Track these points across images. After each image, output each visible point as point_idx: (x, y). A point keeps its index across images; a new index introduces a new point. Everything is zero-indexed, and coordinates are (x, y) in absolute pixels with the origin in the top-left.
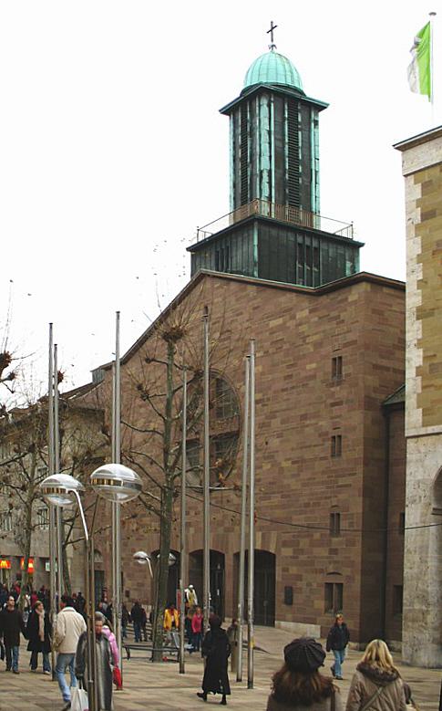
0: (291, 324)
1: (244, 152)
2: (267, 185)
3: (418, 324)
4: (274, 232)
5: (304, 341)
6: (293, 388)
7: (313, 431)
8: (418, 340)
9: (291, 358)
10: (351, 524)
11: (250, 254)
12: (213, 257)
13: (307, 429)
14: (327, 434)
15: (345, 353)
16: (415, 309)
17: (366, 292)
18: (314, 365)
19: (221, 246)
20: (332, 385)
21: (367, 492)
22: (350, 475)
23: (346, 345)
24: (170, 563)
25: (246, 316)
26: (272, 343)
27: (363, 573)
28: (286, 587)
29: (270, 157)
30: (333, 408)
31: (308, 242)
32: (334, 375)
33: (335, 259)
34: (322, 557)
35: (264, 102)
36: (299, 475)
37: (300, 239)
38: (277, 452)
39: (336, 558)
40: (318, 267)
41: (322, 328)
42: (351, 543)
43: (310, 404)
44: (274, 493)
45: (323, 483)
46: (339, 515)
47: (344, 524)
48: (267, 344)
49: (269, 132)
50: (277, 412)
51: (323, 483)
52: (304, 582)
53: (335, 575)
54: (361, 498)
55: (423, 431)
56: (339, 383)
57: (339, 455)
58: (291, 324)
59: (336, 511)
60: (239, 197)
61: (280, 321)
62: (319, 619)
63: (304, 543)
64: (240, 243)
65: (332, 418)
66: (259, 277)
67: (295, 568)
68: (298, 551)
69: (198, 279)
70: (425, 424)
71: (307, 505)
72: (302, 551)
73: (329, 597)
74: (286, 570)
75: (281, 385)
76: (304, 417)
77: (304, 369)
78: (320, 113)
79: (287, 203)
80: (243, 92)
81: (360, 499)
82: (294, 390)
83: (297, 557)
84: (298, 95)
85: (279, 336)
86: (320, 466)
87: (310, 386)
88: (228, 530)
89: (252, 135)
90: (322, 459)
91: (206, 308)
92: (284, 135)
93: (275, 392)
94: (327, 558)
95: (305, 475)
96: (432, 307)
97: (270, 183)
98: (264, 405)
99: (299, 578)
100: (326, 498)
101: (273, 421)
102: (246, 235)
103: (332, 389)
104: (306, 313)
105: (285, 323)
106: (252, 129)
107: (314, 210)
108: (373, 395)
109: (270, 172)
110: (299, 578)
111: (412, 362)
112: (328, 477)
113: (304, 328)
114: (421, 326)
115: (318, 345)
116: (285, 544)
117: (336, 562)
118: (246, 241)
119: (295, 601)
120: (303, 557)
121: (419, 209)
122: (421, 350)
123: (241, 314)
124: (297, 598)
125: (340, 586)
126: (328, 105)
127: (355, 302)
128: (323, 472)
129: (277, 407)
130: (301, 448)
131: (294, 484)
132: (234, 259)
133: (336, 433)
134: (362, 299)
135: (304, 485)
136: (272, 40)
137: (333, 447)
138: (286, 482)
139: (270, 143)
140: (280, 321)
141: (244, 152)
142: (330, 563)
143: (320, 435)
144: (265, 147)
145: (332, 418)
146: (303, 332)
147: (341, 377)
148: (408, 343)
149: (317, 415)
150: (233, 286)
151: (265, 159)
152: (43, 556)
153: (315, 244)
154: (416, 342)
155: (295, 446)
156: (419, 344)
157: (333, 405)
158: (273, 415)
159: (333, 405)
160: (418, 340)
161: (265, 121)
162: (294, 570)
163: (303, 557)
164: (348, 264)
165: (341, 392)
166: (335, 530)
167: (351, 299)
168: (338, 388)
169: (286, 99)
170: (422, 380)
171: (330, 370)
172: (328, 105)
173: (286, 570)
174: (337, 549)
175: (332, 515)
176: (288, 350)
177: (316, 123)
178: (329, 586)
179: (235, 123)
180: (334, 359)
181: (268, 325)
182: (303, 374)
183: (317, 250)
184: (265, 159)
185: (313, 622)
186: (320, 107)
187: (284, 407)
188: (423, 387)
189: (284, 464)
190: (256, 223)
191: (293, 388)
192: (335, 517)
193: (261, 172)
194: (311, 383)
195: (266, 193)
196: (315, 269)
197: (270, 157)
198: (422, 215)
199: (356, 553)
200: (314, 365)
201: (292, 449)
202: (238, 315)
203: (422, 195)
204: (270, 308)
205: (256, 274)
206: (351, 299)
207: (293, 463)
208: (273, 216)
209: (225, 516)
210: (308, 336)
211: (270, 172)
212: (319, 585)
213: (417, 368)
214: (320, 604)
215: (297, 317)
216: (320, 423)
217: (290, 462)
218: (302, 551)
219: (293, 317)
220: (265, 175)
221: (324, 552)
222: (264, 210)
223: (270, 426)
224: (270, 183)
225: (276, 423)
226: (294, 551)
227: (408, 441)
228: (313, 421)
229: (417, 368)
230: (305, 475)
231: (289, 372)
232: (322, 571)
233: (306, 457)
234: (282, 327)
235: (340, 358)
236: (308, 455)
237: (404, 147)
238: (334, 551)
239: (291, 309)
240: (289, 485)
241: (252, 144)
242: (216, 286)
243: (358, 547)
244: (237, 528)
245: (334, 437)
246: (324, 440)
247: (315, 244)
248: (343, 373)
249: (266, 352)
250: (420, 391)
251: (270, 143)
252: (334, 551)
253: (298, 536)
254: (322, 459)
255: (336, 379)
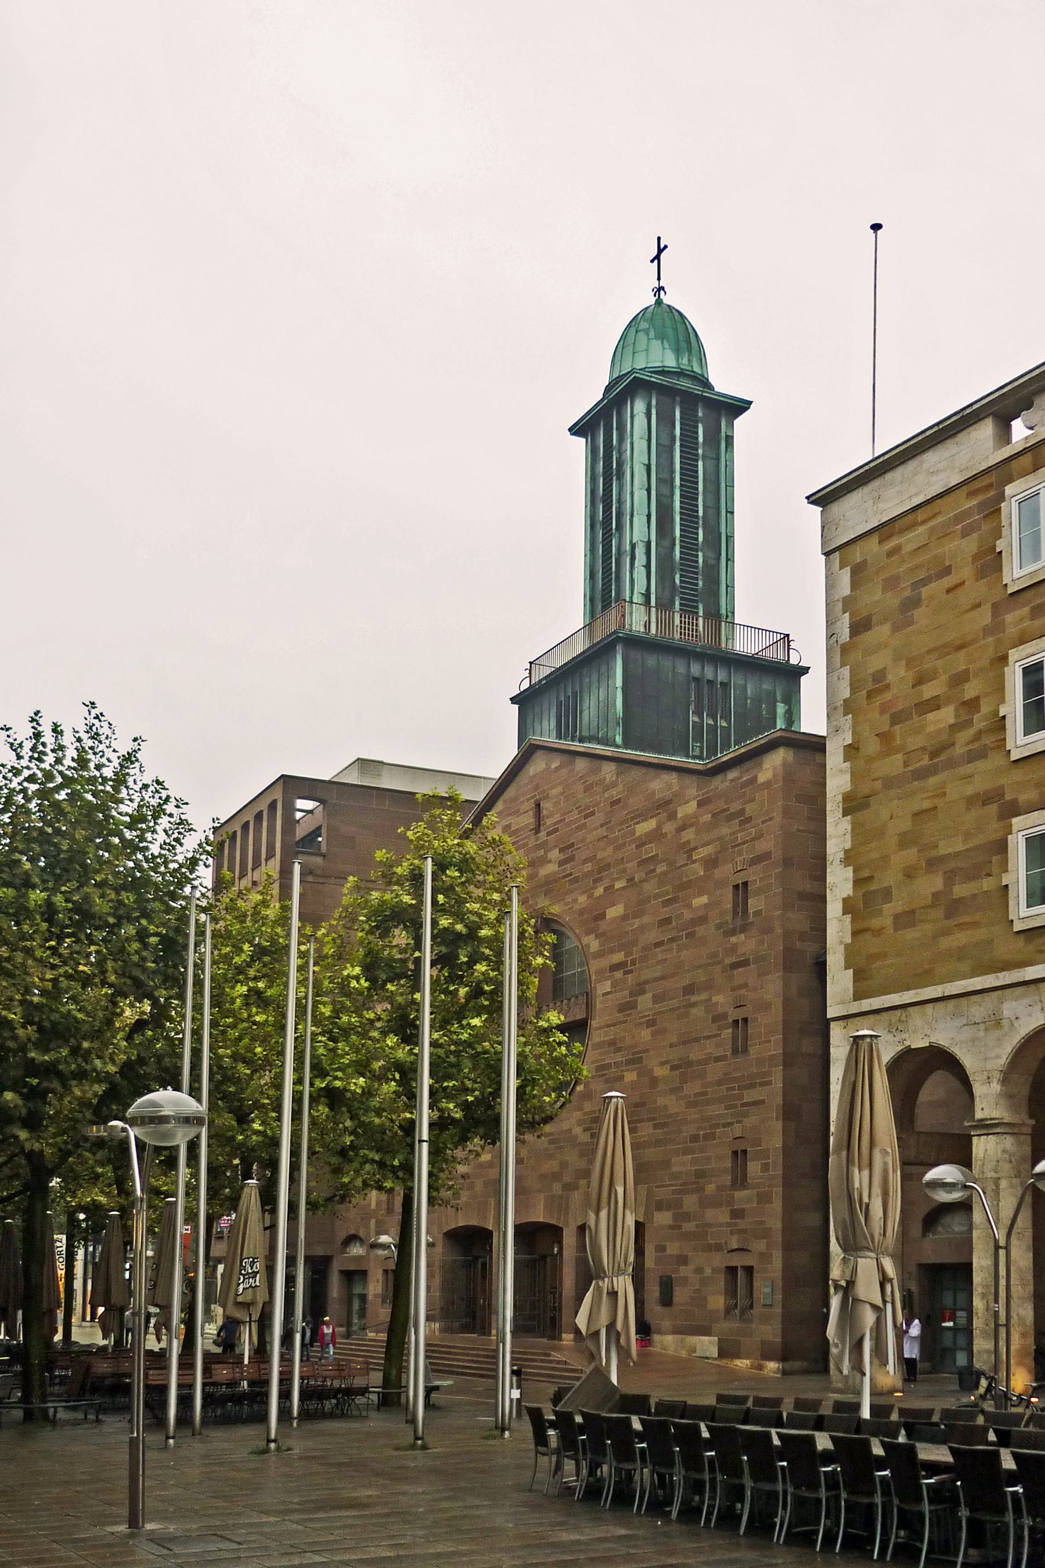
0: (669, 828)
1: (607, 508)
2: (643, 570)
3: (846, 824)
4: (651, 660)
5: (690, 857)
6: (672, 940)
7: (702, 1013)
8: (846, 852)
9: (669, 888)
10: (765, 1167)
11: (609, 704)
12: (553, 711)
13: (694, 1011)
14: (724, 1016)
15: (754, 875)
16: (840, 798)
17: (785, 764)
18: (704, 899)
19: (565, 692)
20: (733, 932)
21: (789, 1112)
22: (762, 1084)
23: (756, 861)
24: (84, 1225)
25: (599, 817)
26: (640, 864)
27: (788, 1247)
28: (661, 1277)
29: (649, 516)
30: (735, 972)
31: (709, 673)
32: (735, 912)
33: (758, 701)
34: (721, 1225)
35: (640, 406)
36: (679, 1089)
37: (695, 669)
38: (647, 1051)
39: (742, 1224)
40: (726, 717)
41: (715, 833)
42: (764, 1198)
43: (700, 967)
44: (641, 1121)
45: (720, 1100)
46: (745, 1152)
47: (754, 1168)
48: (631, 865)
49: (648, 468)
50: (647, 982)
51: (720, 1100)
52: (691, 1267)
53: (742, 1253)
54: (781, 1122)
55: (855, 1008)
56: (744, 929)
57: (745, 1050)
58: (669, 828)
59: (740, 1146)
60: (598, 596)
61: (651, 824)
62: (716, 1327)
63: (690, 1202)
64: (595, 684)
65: (733, 989)
66: (626, 744)
67: (676, 1244)
68: (682, 1217)
69: (527, 753)
70: (858, 996)
71: (695, 1138)
72: (687, 1217)
73: (731, 1291)
74: (661, 1249)
75: (653, 936)
76: (690, 989)
77: (689, 905)
78: (738, 422)
79: (677, 603)
80: (608, 389)
81: (778, 1125)
82: (674, 945)
83: (680, 1227)
84: (697, 389)
85: (652, 850)
86: (714, 1071)
87: (699, 935)
88: (570, 1187)
89: (620, 475)
90: (718, 1059)
91: (538, 805)
92: (673, 472)
93: (644, 949)
94: (728, 1225)
95: (693, 1088)
96: (867, 792)
97: (648, 567)
98: (625, 973)
99: (683, 1260)
100: (724, 1125)
101: (640, 999)
102: (604, 669)
103: (734, 939)
104: (692, 807)
105: (659, 827)
106: (620, 464)
107: (723, 611)
108: (798, 945)
109: (648, 544)
110: (683, 1260)
111: (837, 891)
112: (728, 1089)
113: (688, 835)
114: (849, 827)
115: (711, 863)
116: (660, 1206)
117: (743, 1231)
118: (604, 684)
119: (676, 1300)
120: (689, 1227)
121: (847, 614)
122: (850, 869)
123: (593, 814)
124: (680, 1295)
125: (749, 1270)
126: (750, 403)
127: (768, 784)
128: (719, 1083)
129: (648, 974)
130: (685, 1043)
131: (671, 1103)
132: (586, 713)
133: (739, 1014)
134: (780, 778)
135: (692, 1104)
136: (659, 279)
137: (735, 1039)
138: (661, 1101)
139: (649, 490)
140: (651, 824)
141: (607, 508)
142: (732, 1233)
143: (715, 1019)
144: (640, 495)
145: (733, 989)
146: (688, 842)
147: (748, 917)
148: (829, 858)
149: (709, 986)
150: (581, 764)
151: (639, 521)
152: (933, 1259)
153: (722, 676)
154: (842, 855)
155: (675, 1040)
156: (848, 859)
157: (735, 966)
158: (639, 990)
159: (735, 966)
160: (846, 852)
161: (640, 445)
162: (673, 1249)
163: (689, 1227)
164: (781, 709)
165: (746, 943)
166: (740, 1179)
167: (762, 778)
168: (742, 937)
169: (678, 399)
170: (853, 921)
171: (730, 906)
172: (750, 403)
173: (661, 1249)
174: (743, 1210)
175: (735, 1153)
176: (665, 874)
177: (730, 440)
178: (732, 1270)
179: (593, 451)
180: (736, 887)
181: (633, 832)
182: (688, 915)
183: (725, 685)
184: (639, 521)
185: (706, 1331)
186: (739, 407)
187: (658, 974)
188: (855, 934)
189: (660, 1072)
190: (619, 649)
191: (672, 940)
192: (740, 1156)
193: (633, 547)
194: (700, 931)
195: (640, 586)
196: (708, 721)
197: (649, 516)
198: (851, 627)
199: (774, 1217)
200: (704, 899)
201: (671, 1046)
202: (586, 817)
203: (851, 591)
204: (637, 802)
205: (619, 740)
206: (762, 778)
207: (673, 1068)
208: (653, 631)
209: (563, 1165)
210: (696, 848)
211: (648, 544)
212: (714, 1270)
213: (845, 900)
214: (718, 1302)
215: (679, 816)
216: (715, 999)
217: (668, 1066)
218: (687, 1217)
219: (672, 816)
220: (640, 552)
221: (722, 1216)
222: (637, 620)
223: (635, 1007)
224: (648, 567)
225: (645, 1002)
226: (675, 1217)
227: (833, 1025)
228: (703, 996)
229: (845, 900)
230: (693, 1088)
231: (666, 912)
232: (718, 1248)
233: (692, 1057)
234: (656, 835)
235: (745, 884)
236: (695, 1054)
237: (823, 499)
238: (738, 1214)
239: (668, 802)
240: (666, 1107)
241: (619, 494)
242: (553, 766)
243: (777, 1205)
244: (583, 1183)
245: (736, 1022)
246: (720, 1028)
247: (722, 676)
248: (751, 911)
249: (631, 880)
250: (849, 940)
251: (649, 490)
252: (738, 1214)
253: (680, 1192)
254: (718, 1059)
255: (739, 922)
